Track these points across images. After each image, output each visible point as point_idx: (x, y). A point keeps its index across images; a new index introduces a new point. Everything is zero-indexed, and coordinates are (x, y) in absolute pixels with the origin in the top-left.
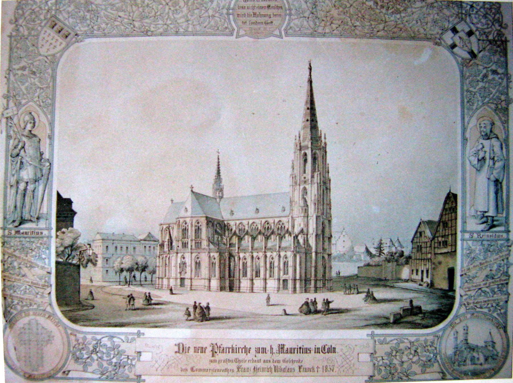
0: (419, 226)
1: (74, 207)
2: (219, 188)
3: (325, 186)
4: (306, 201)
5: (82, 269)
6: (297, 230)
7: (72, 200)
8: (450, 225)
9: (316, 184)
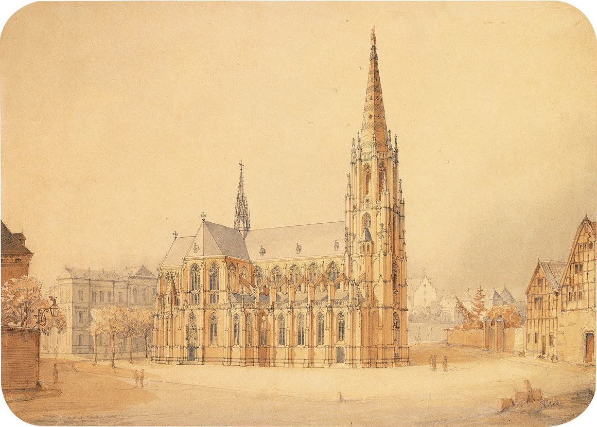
0: (536, 272)
1: (28, 245)
2: (242, 213)
3: (396, 215)
4: (368, 235)
5: (42, 336)
6: (356, 276)
7: (26, 236)
8: (585, 268)
9: (384, 209)
